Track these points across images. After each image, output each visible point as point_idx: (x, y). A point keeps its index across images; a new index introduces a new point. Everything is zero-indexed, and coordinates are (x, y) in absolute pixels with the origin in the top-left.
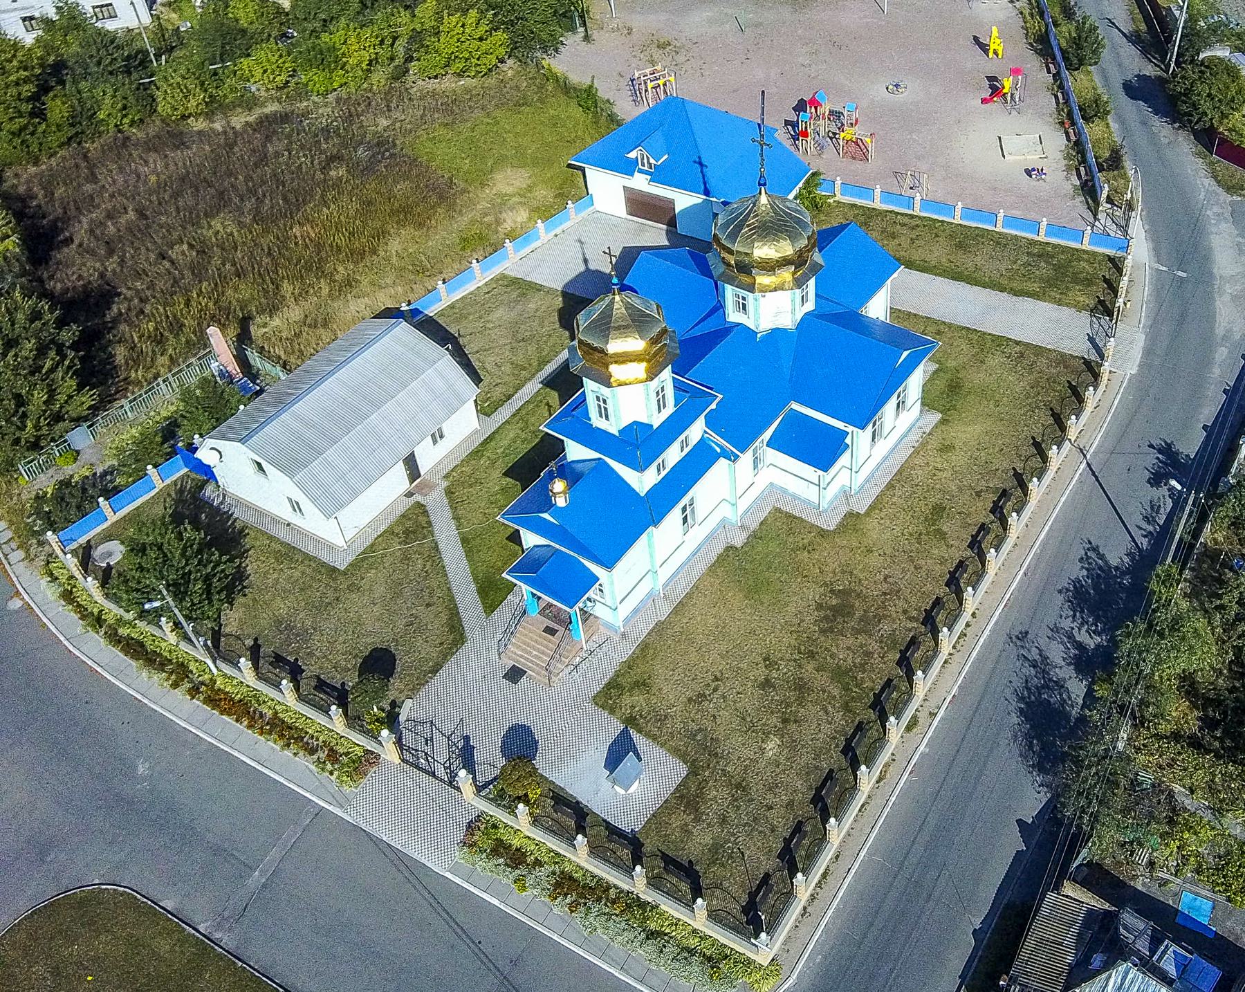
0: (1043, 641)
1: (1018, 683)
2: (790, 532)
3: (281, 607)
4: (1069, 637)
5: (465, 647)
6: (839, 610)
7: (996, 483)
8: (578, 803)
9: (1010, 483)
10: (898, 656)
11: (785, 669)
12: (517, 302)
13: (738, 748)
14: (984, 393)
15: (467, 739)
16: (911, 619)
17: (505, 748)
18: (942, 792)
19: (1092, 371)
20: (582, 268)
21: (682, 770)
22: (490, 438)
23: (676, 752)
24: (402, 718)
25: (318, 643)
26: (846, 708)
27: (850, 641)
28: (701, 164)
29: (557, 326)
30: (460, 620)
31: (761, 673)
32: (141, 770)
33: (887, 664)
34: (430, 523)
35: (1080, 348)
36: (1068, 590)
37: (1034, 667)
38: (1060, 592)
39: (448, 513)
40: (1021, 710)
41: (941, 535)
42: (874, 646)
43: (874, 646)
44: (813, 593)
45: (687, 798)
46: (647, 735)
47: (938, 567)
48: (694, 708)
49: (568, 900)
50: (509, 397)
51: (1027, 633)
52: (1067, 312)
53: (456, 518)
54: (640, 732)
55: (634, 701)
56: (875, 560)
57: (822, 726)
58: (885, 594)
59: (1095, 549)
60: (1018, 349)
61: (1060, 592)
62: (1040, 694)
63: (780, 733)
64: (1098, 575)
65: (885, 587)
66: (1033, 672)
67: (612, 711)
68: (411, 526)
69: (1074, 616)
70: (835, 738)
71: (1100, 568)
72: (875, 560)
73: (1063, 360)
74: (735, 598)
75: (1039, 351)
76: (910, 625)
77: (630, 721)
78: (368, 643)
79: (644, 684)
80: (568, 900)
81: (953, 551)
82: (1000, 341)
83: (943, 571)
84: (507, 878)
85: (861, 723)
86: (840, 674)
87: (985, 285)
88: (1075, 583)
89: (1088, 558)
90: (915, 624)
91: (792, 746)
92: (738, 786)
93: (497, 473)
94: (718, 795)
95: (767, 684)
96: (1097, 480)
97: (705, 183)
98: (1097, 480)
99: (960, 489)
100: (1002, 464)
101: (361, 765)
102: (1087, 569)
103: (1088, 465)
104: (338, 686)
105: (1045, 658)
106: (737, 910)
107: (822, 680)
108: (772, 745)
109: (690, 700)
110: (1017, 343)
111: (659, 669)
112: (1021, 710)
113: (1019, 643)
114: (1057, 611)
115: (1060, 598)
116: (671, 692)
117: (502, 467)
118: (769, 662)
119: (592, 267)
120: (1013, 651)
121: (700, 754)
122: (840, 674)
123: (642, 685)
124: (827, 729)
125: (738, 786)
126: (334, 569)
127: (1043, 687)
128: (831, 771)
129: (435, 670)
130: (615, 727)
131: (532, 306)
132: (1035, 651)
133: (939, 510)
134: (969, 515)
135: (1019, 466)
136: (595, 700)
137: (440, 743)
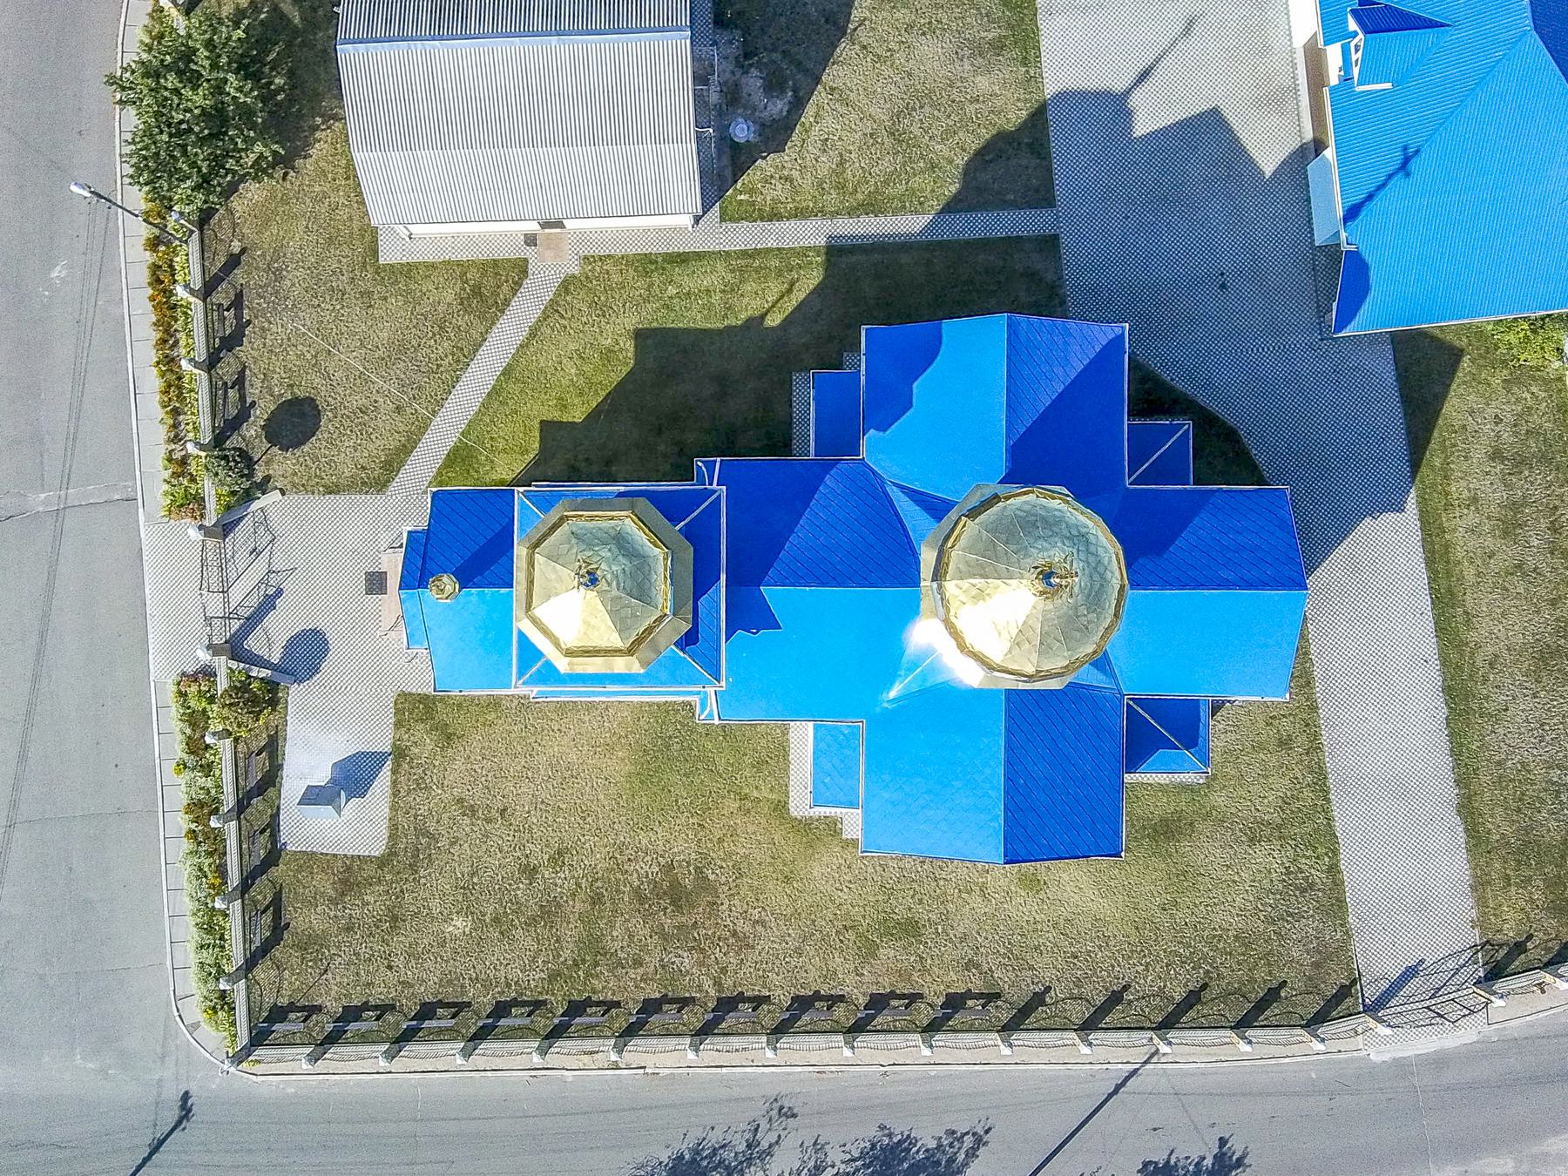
0: (791, 1142)
1: (715, 1138)
2: (759, 765)
3: (298, 239)
4: (816, 1167)
5: (372, 500)
6: (677, 893)
7: (1003, 978)
8: (281, 766)
9: (1018, 994)
10: (658, 995)
11: (562, 881)
12: (978, 50)
13: (437, 884)
14: (1184, 876)
15: (279, 592)
16: (717, 983)
17: (293, 644)
18: (531, 1121)
19: (1335, 1003)
20: (1119, 86)
21: (378, 848)
22: (681, 259)
23: (394, 829)
24: (255, 506)
25: (280, 328)
26: (553, 976)
27: (643, 932)
28: (1406, 161)
29: (961, 161)
30: (402, 463)
31: (539, 854)
32: (54, 274)
33: (633, 989)
34: (507, 303)
35: (1377, 960)
36: (890, 1135)
37: (749, 1146)
38: (882, 1128)
39: (535, 314)
40: (682, 1157)
41: (871, 951)
42: (652, 961)
43: (652, 961)
44: (683, 849)
45: (350, 876)
46: (394, 783)
47: (813, 973)
48: (455, 811)
49: (193, 826)
50: (775, 216)
51: (794, 1116)
52: (1466, 908)
53: (533, 333)
54: (394, 772)
55: (424, 743)
56: (777, 895)
57: (515, 965)
58: (734, 934)
59: (979, 1141)
60: (1318, 876)
61: (882, 1128)
62: (715, 1169)
63: (479, 923)
64: (938, 1163)
65: (743, 927)
66: (742, 1147)
67: (398, 725)
68: (487, 285)
69: (854, 1160)
70: (508, 985)
71: (951, 1160)
72: (777, 895)
73: (1335, 952)
74: (619, 766)
75: (1335, 906)
76: (708, 985)
77: (399, 753)
78: (311, 384)
79: (449, 737)
80: (193, 826)
81: (851, 980)
82: (1325, 840)
83: (813, 982)
84: (179, 751)
85: (544, 1002)
86: (593, 948)
87: (1457, 749)
88: (909, 1140)
89: (960, 1139)
90: (712, 993)
91: (477, 942)
92: (395, 919)
93: (631, 321)
94: (374, 901)
95: (530, 872)
96: (1110, 1096)
97: (1370, 197)
98: (1110, 1096)
99: (964, 938)
100: (1047, 970)
101: (190, 503)
102: (940, 1146)
103: (1136, 1071)
104: (249, 400)
105: (769, 1152)
106: (269, 1000)
107: (571, 931)
108: (460, 924)
109: (460, 801)
110: (1333, 870)
111: (476, 740)
112: (682, 1157)
113: (774, 1113)
114: (864, 1133)
115: (872, 1132)
116: (456, 773)
117: (651, 316)
118: (558, 858)
119: (1135, 100)
120: (757, 1111)
121: (409, 852)
122: (593, 948)
123: (448, 737)
124: (516, 973)
125: (395, 919)
126: (375, 253)
127: (727, 1168)
128: (469, 1004)
129: (332, 490)
130: (383, 742)
131: (983, 83)
132: (773, 1137)
133: (910, 929)
134: (925, 971)
135: (1058, 992)
136: (404, 696)
137: (260, 566)
